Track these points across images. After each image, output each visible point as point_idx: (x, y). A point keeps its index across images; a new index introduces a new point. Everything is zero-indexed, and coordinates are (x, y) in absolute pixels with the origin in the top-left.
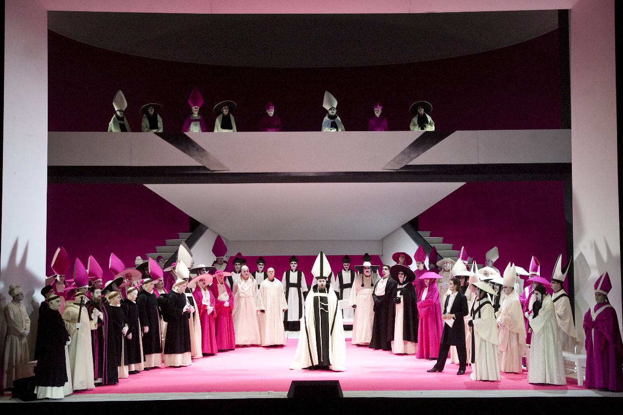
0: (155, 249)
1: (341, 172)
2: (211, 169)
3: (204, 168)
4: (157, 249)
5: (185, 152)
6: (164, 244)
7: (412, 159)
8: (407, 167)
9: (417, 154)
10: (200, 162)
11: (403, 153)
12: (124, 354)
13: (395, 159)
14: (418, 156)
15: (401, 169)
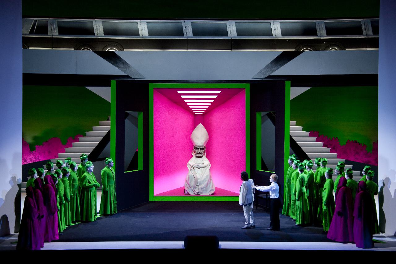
0: (92, 128)
1: (223, 80)
2: (133, 77)
3: (127, 76)
4: (73, 145)
5: (114, 65)
6: (64, 152)
7: (273, 71)
8: (269, 77)
9: (277, 68)
10: (125, 72)
11: (267, 67)
12: (329, 39)
13: (261, 71)
14: (277, 69)
15: (265, 78)
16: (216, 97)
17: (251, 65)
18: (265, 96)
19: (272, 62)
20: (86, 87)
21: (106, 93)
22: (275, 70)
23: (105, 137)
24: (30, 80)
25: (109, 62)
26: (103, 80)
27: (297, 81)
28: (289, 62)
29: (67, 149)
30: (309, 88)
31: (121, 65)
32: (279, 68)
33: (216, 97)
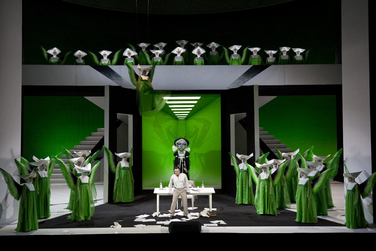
5: (108, 77)
7: (245, 82)
10: (118, 83)
11: (239, 78)
14: (248, 80)
16: (196, 102)
17: (226, 77)
18: (234, 101)
19: (243, 74)
20: (87, 98)
21: (103, 102)
22: (247, 81)
23: (96, 145)
24: (29, 92)
25: (104, 75)
26: (98, 91)
27: (265, 90)
28: (258, 74)
29: (93, 133)
30: (275, 97)
31: (115, 78)
32: (250, 79)
33: (196, 102)
